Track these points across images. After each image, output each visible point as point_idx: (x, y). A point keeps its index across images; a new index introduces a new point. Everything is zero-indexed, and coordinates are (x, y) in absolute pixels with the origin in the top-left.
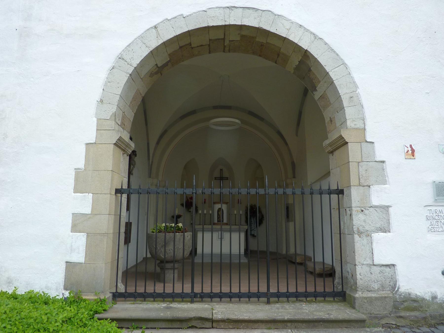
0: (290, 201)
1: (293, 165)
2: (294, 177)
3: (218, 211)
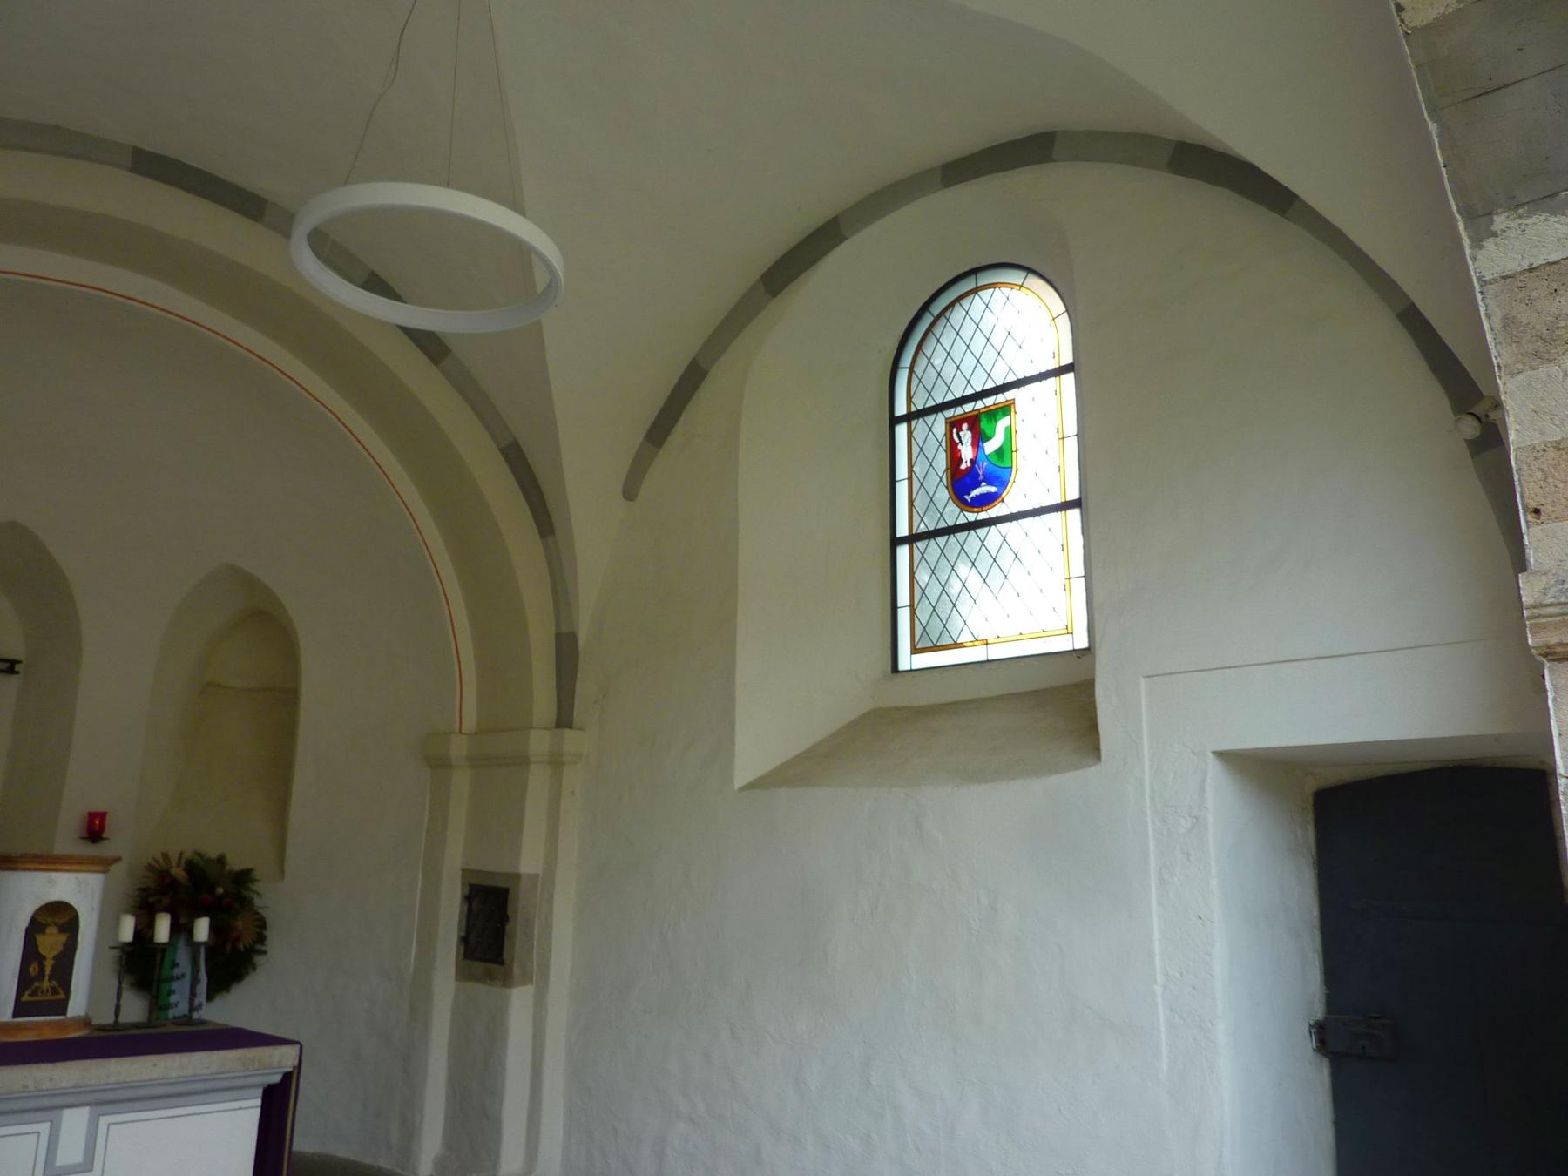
0: (529, 862)
1: (566, 650)
2: (564, 720)
3: (35, 927)
